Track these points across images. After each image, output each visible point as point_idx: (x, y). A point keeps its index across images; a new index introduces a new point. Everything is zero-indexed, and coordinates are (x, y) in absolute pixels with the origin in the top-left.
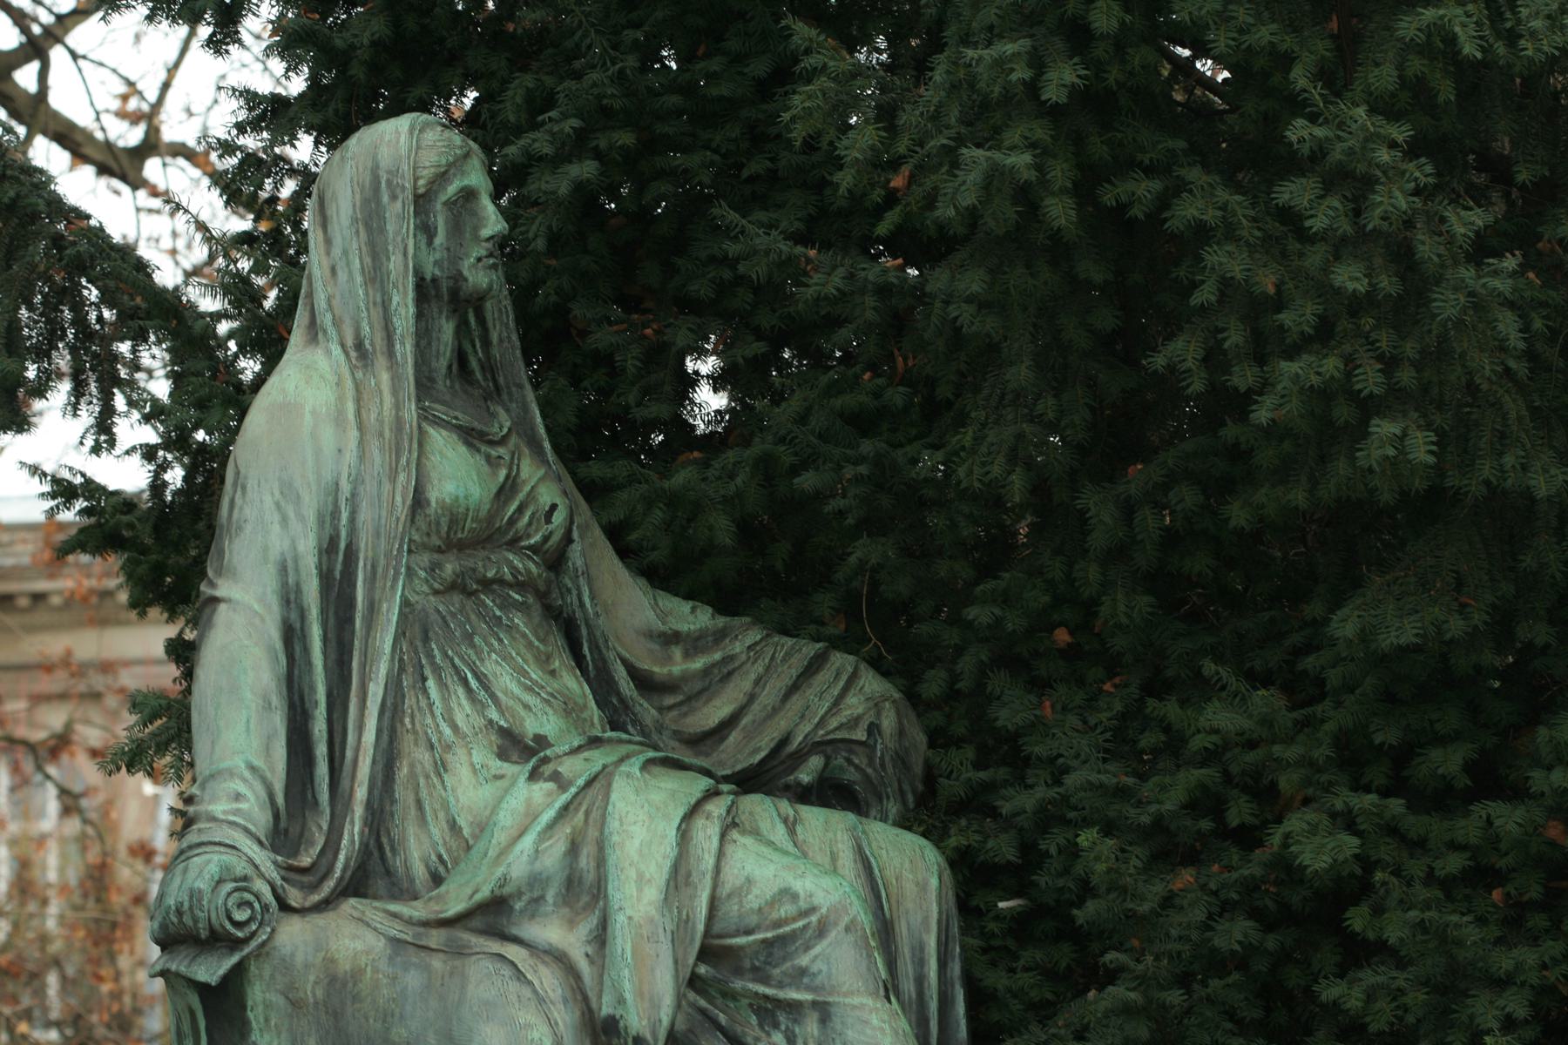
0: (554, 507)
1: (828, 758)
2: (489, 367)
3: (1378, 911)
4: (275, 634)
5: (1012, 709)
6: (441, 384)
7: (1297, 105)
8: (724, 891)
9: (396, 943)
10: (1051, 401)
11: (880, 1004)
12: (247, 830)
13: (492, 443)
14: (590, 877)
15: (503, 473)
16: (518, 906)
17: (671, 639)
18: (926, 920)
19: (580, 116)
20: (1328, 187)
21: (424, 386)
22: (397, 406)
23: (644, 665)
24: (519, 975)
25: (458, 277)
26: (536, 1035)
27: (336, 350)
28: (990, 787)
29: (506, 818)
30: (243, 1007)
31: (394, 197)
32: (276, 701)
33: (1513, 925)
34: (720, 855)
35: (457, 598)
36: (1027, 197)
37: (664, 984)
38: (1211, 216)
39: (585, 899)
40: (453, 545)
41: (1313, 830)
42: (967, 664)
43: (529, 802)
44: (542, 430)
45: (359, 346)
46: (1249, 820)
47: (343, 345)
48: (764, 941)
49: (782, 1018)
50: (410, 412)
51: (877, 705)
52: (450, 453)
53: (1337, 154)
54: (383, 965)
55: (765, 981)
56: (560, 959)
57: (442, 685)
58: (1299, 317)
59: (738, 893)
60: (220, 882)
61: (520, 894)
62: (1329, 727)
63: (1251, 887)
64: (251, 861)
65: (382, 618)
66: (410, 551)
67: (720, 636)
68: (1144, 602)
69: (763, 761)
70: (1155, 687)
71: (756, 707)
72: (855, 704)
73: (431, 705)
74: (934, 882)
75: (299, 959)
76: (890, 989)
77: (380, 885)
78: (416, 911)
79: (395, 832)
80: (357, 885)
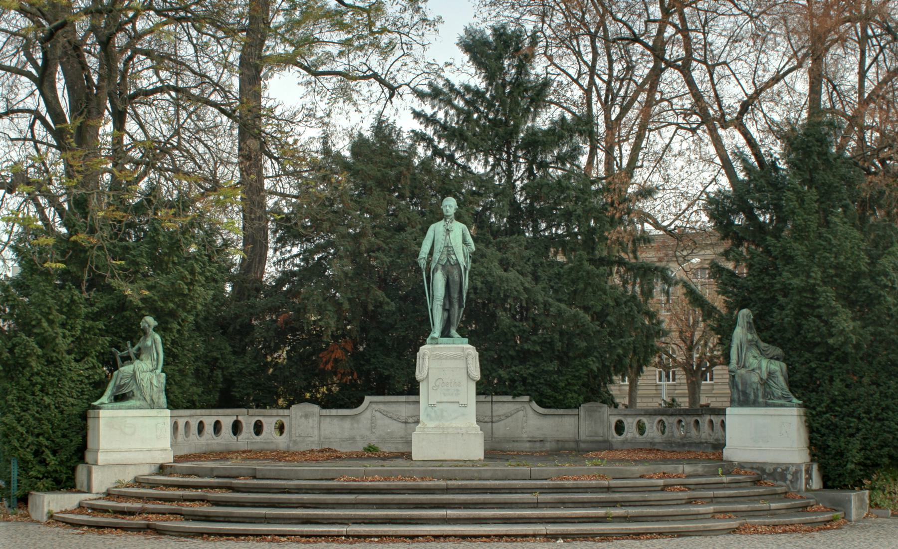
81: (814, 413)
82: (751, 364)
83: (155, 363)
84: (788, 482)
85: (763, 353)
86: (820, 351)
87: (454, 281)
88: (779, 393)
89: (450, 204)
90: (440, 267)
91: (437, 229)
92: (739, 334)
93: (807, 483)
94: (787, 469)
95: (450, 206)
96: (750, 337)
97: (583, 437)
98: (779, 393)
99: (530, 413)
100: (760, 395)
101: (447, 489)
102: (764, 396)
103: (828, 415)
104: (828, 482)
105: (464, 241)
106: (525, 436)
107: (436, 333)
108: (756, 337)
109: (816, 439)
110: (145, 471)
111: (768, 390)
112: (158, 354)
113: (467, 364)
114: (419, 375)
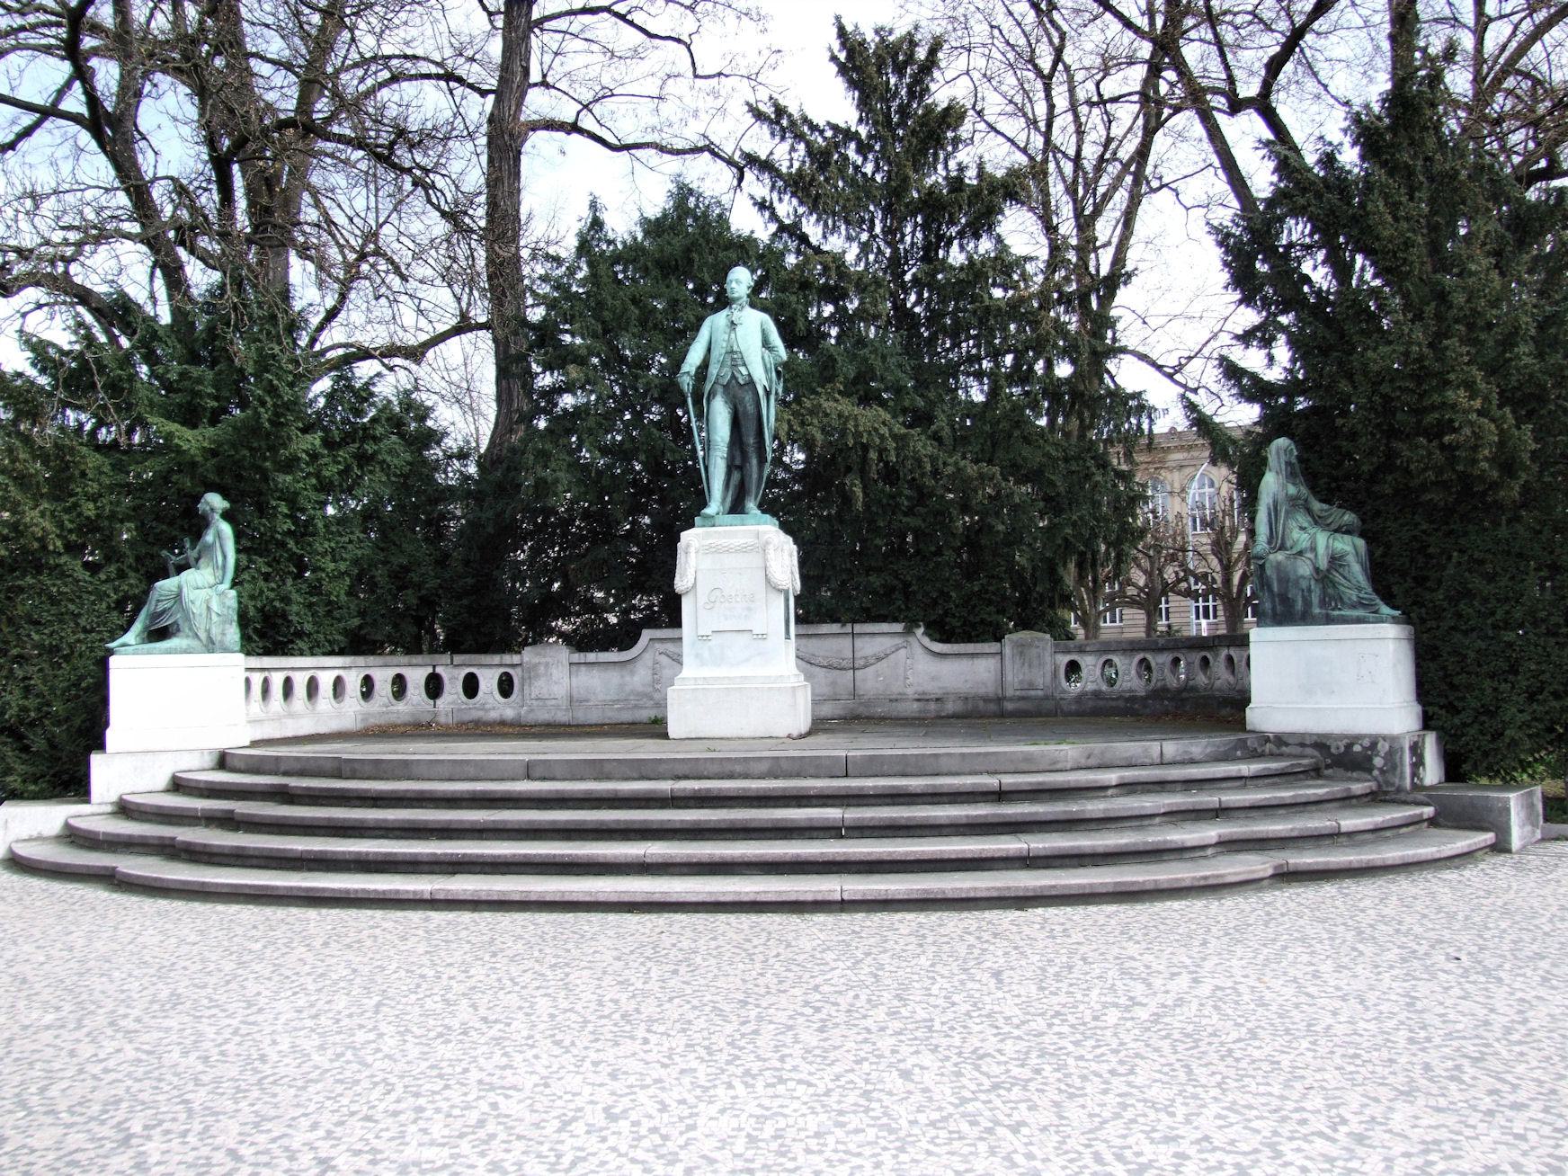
82: (1295, 543)
83: (219, 573)
84: (1376, 773)
85: (1318, 521)
87: (745, 412)
88: (1353, 595)
89: (741, 279)
90: (720, 389)
91: (717, 321)
92: (1271, 484)
93: (1414, 774)
94: (1374, 745)
95: (738, 282)
96: (1292, 490)
97: (1010, 693)
98: (1353, 595)
99: (919, 651)
100: (1315, 599)
101: (673, 798)
102: (1323, 604)
104: (1454, 770)
105: (766, 344)
106: (910, 691)
107: (713, 508)
108: (1304, 491)
110: (197, 767)
111: (1330, 591)
112: (225, 557)
113: (766, 560)
114: (680, 584)
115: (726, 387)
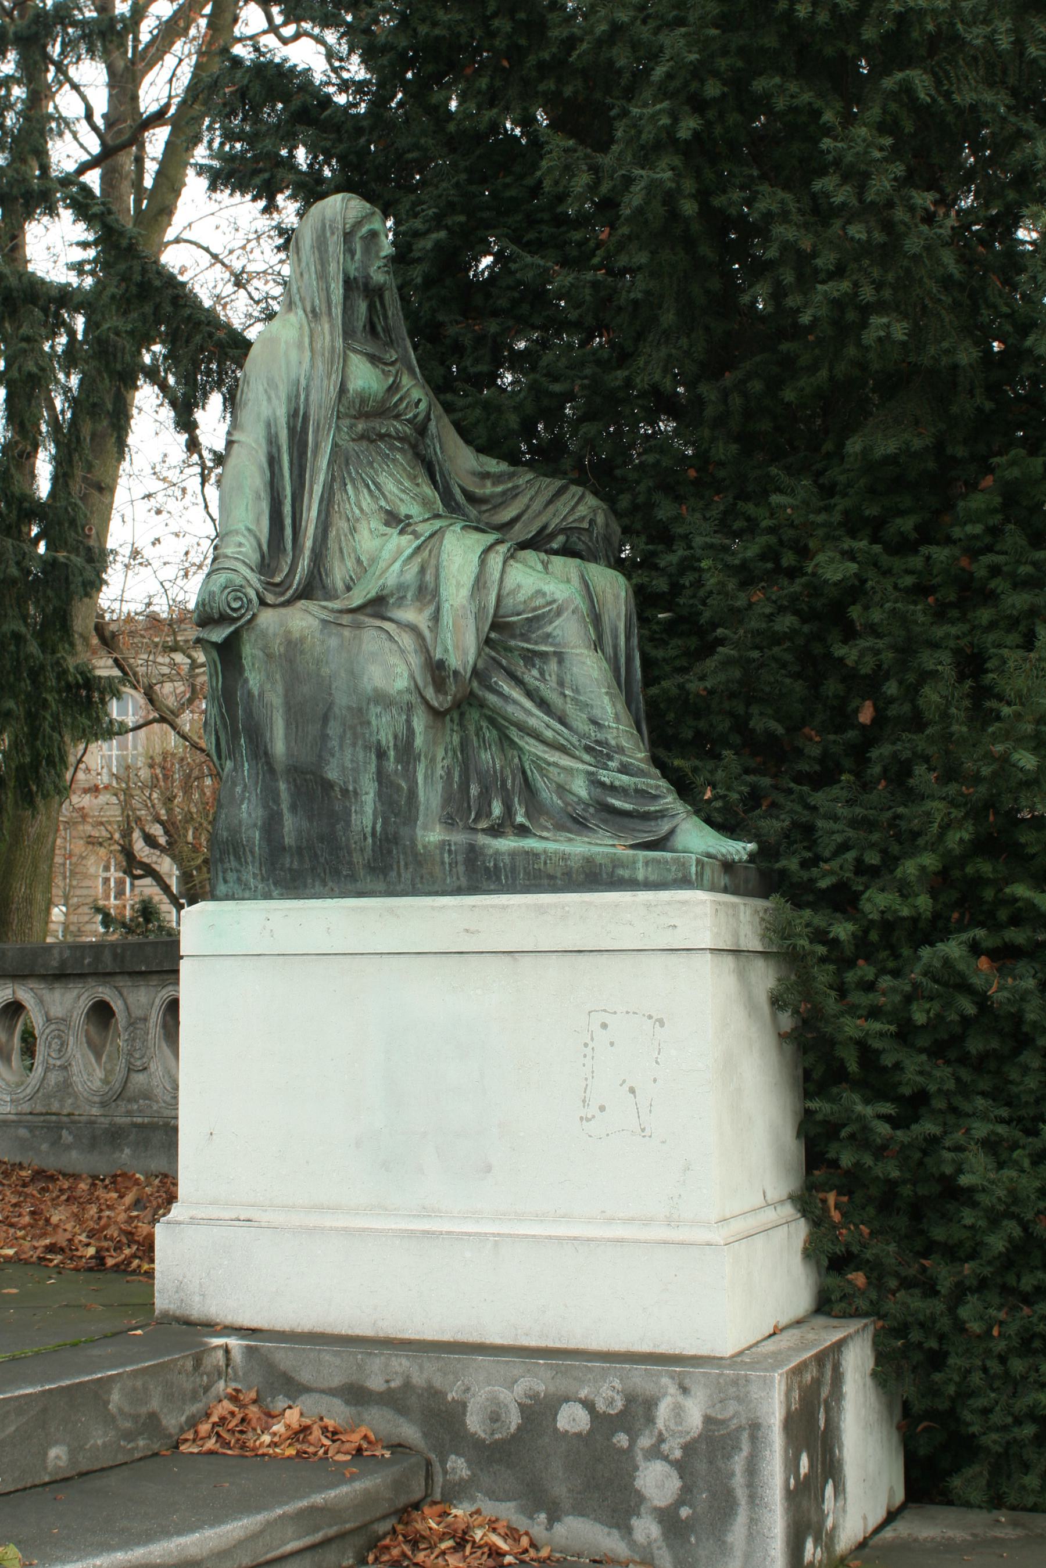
0: (420, 400)
1: (568, 538)
2: (387, 330)
3: (866, 608)
4: (263, 460)
5: (665, 511)
6: (359, 334)
7: (827, 131)
8: (505, 592)
9: (325, 622)
10: (685, 340)
11: (592, 653)
12: (244, 563)
13: (386, 364)
14: (431, 586)
15: (391, 380)
16: (391, 601)
17: (485, 476)
18: (618, 615)
19: (437, 207)
20: (845, 178)
21: (348, 333)
22: (332, 341)
23: (471, 488)
24: (391, 638)
25: (368, 277)
26: (399, 670)
27: (300, 312)
28: (654, 554)
29: (386, 555)
30: (240, 658)
31: (333, 233)
32: (263, 495)
33: (940, 615)
34: (503, 572)
35: (365, 443)
36: (670, 198)
37: (470, 642)
38: (775, 208)
39: (429, 597)
40: (363, 415)
41: (832, 560)
42: (642, 488)
43: (398, 546)
44: (415, 362)
45: (313, 311)
46: (793, 563)
47: (305, 311)
48: (527, 619)
49: (537, 661)
50: (339, 343)
51: (594, 511)
52: (361, 366)
53: (849, 158)
54: (317, 634)
55: (528, 641)
56: (413, 629)
57: (355, 487)
58: (826, 260)
59: (513, 592)
60: (226, 587)
61: (392, 594)
62: (838, 508)
63: (794, 598)
64: (245, 578)
65: (321, 451)
66: (338, 418)
67: (511, 476)
68: (734, 448)
69: (533, 537)
70: (743, 496)
71: (530, 511)
72: (582, 510)
73: (349, 498)
74: (623, 594)
75: (271, 631)
76: (598, 645)
77: (319, 593)
78: (336, 605)
79: (327, 565)
80: (306, 592)
81: (843, 930)
86: (887, 446)
103: (953, 948)
109: (862, 1140)
111: (488, 758)
115: (40, 379)
